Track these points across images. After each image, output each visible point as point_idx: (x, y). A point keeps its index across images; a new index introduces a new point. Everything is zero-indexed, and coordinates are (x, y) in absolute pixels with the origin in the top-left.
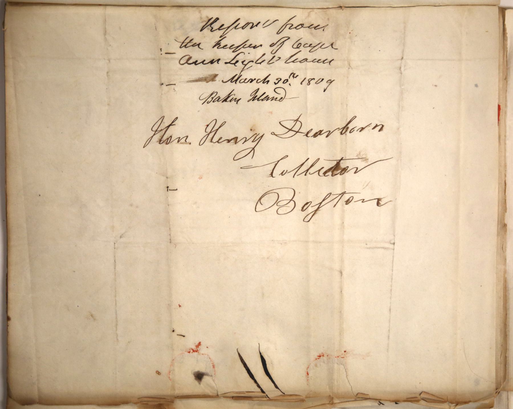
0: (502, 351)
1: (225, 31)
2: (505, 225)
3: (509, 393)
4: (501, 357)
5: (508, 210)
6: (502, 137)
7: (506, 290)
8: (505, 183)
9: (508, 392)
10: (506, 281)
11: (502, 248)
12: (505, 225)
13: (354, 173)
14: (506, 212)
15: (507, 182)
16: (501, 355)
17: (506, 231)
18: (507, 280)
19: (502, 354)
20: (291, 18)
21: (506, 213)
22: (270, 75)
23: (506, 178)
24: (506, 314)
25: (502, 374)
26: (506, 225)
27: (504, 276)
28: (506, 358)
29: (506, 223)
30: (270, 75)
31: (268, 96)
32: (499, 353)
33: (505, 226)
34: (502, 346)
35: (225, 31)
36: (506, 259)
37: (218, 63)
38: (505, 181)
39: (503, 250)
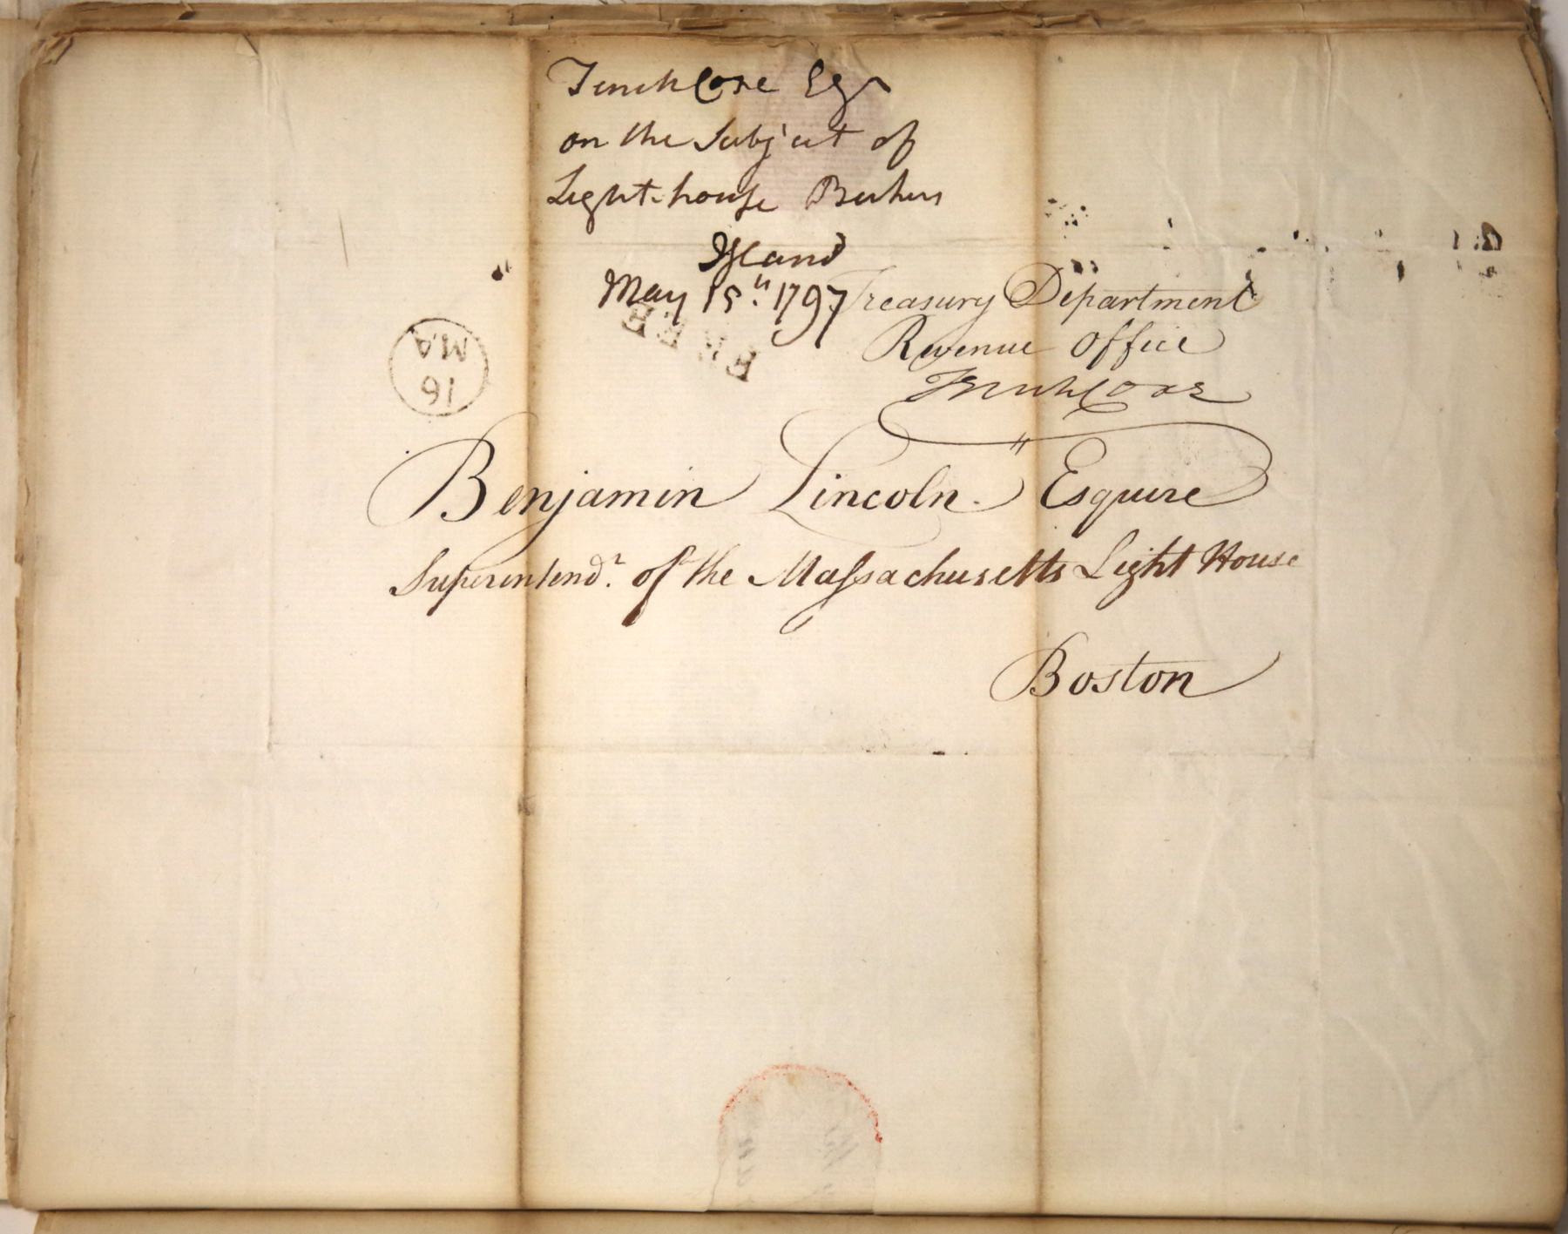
0: (32, 176)
1: (1069, 385)
2: (19, 558)
3: (16, 15)
4: (37, 155)
6: (24, 713)
7: (19, 359)
8: (19, 688)
9: (19, 18)
10: (19, 386)
11: (30, 490)
12: (20, 559)
13: (1486, 220)
14: (17, 600)
16: (35, 164)
18: (16, 388)
19: (31, 167)
20: (423, 511)
21: (18, 595)
22: (1107, 380)
23: (16, 704)
24: (18, 283)
25: (33, 105)
26: (16, 560)
27: (24, 402)
28: (21, 150)
29: (17, 568)
30: (1107, 380)
31: (656, 286)
32: (40, 170)
35: (1069, 385)
36: (20, 453)
37: (840, 235)
38: (19, 695)
39: (28, 489)
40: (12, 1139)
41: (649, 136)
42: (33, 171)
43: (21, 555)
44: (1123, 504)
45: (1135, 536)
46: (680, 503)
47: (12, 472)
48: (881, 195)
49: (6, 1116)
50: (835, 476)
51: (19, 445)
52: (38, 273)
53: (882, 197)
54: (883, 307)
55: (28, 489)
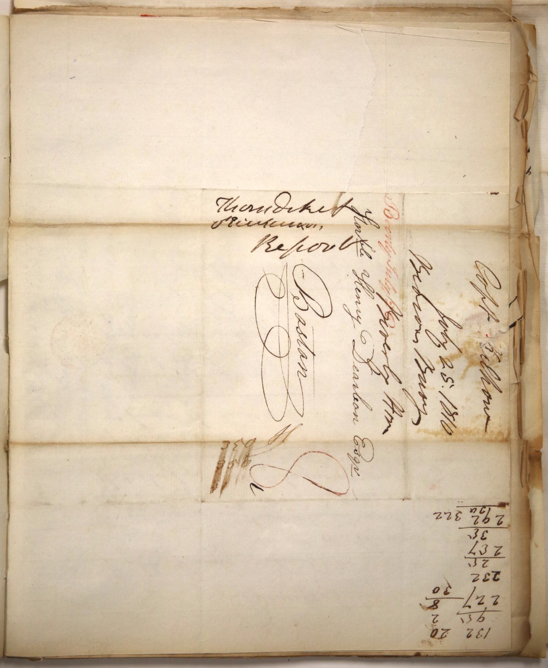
0: (452, 13)
1: (487, 297)
2: (297, 9)
4: (469, 15)
5: (277, 5)
12: (297, 9)
14: (279, 8)
15: (239, 7)
17: (304, 7)
21: (281, 8)
25: (491, 13)
26: (296, 7)
27: (363, 10)
32: (464, 17)
33: (297, 10)
34: (453, 13)
35: (487, 297)
38: (239, 9)
39: (328, 12)
40: (55, 9)
41: (354, 458)
42: (463, 14)
43: (298, 9)
44: (352, 271)
45: (354, 317)
46: (443, 397)
47: (333, 5)
48: (499, 286)
49: (62, 6)
50: (471, 517)
51: (344, 8)
52: (421, 16)
53: (355, 411)
54: (358, 462)
55: (328, 12)
